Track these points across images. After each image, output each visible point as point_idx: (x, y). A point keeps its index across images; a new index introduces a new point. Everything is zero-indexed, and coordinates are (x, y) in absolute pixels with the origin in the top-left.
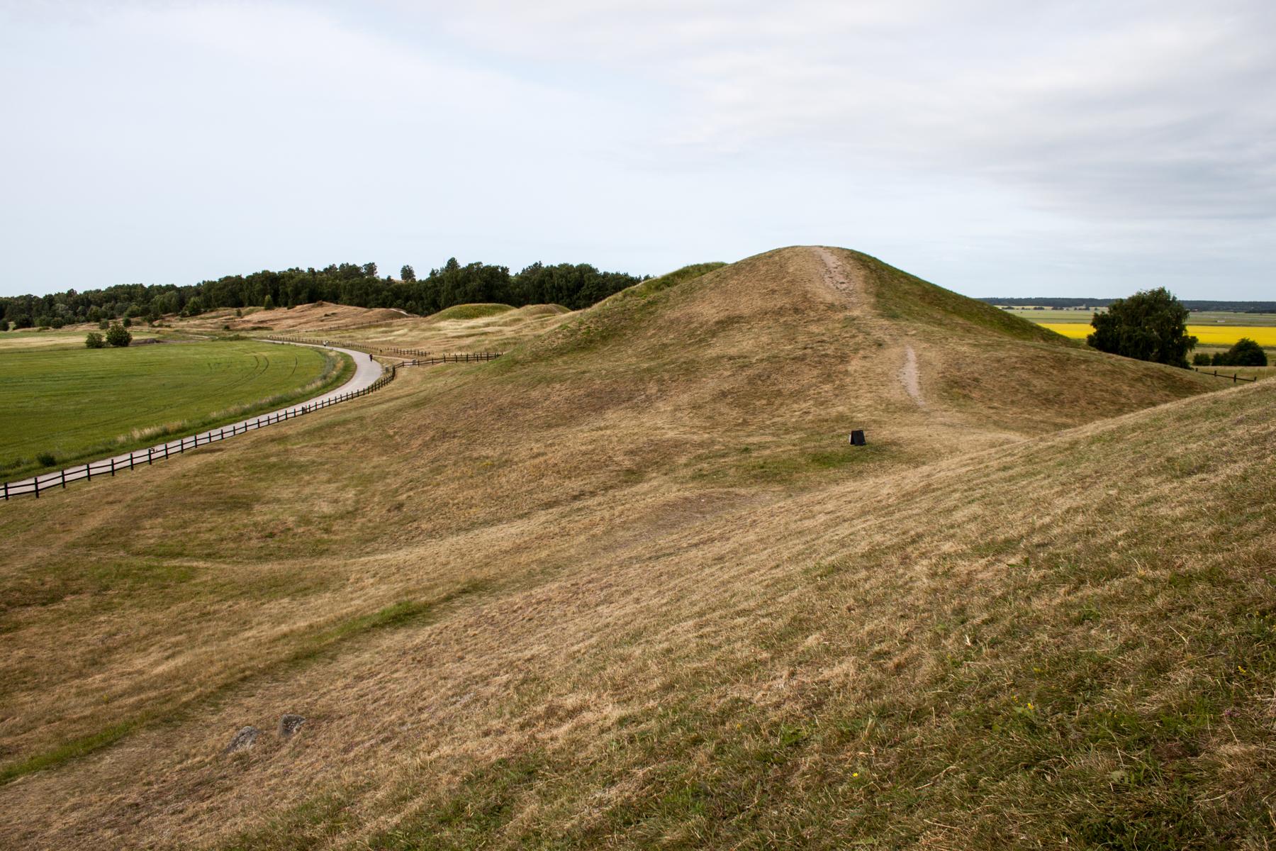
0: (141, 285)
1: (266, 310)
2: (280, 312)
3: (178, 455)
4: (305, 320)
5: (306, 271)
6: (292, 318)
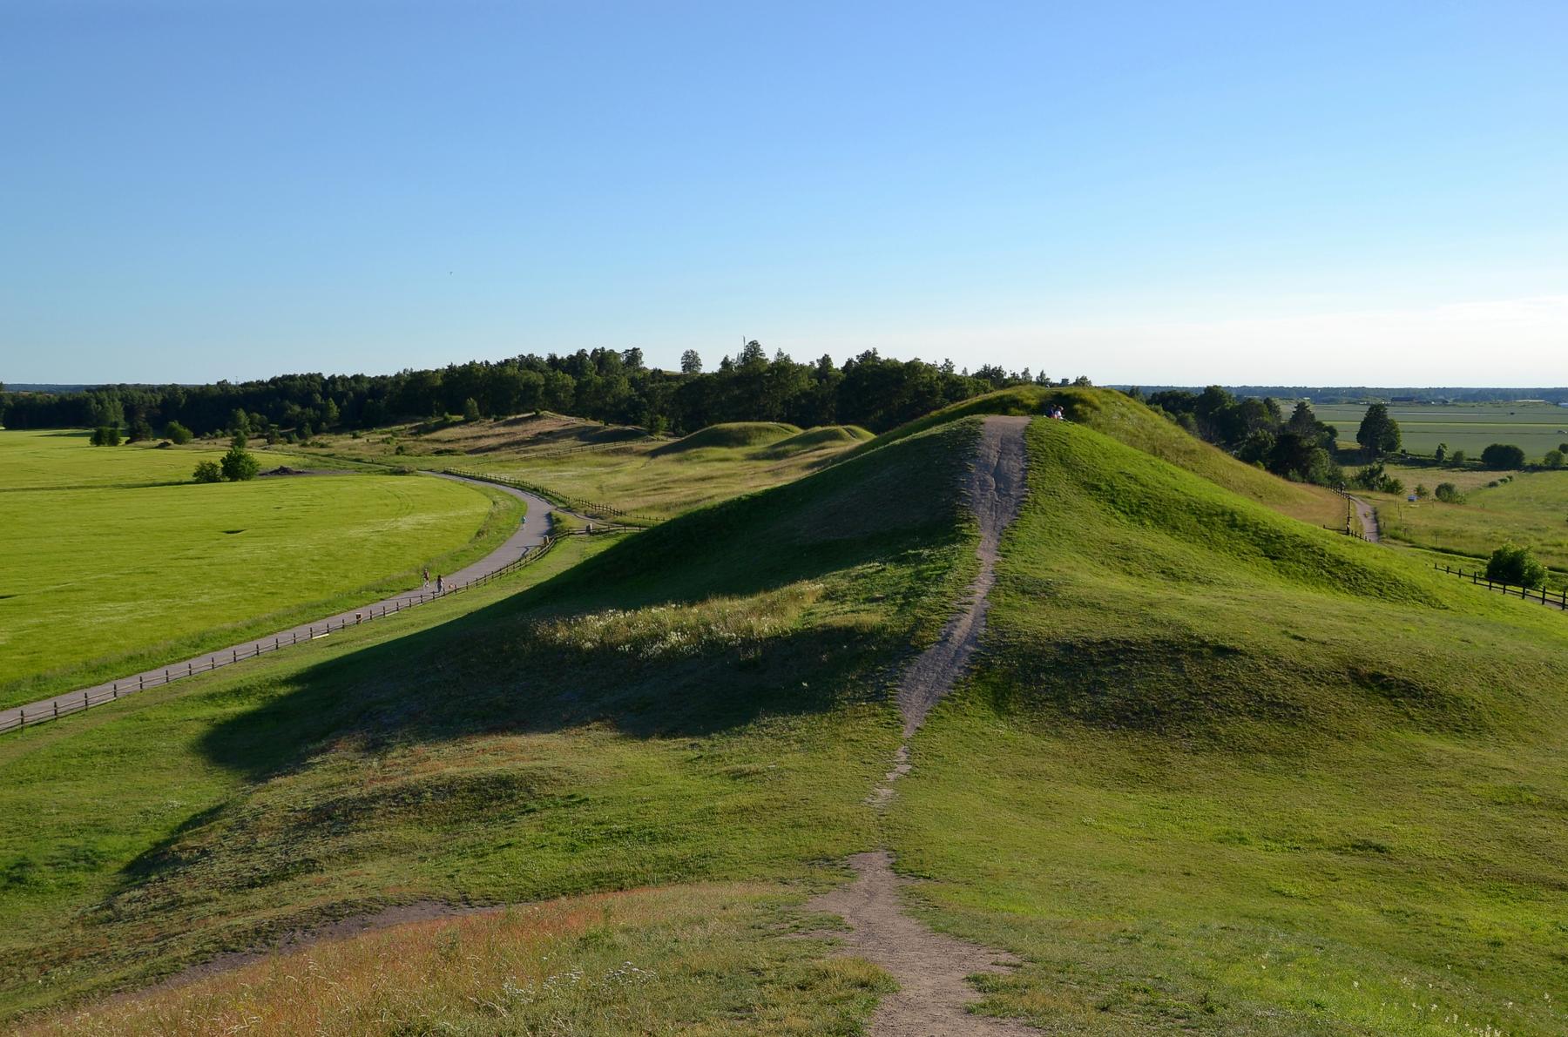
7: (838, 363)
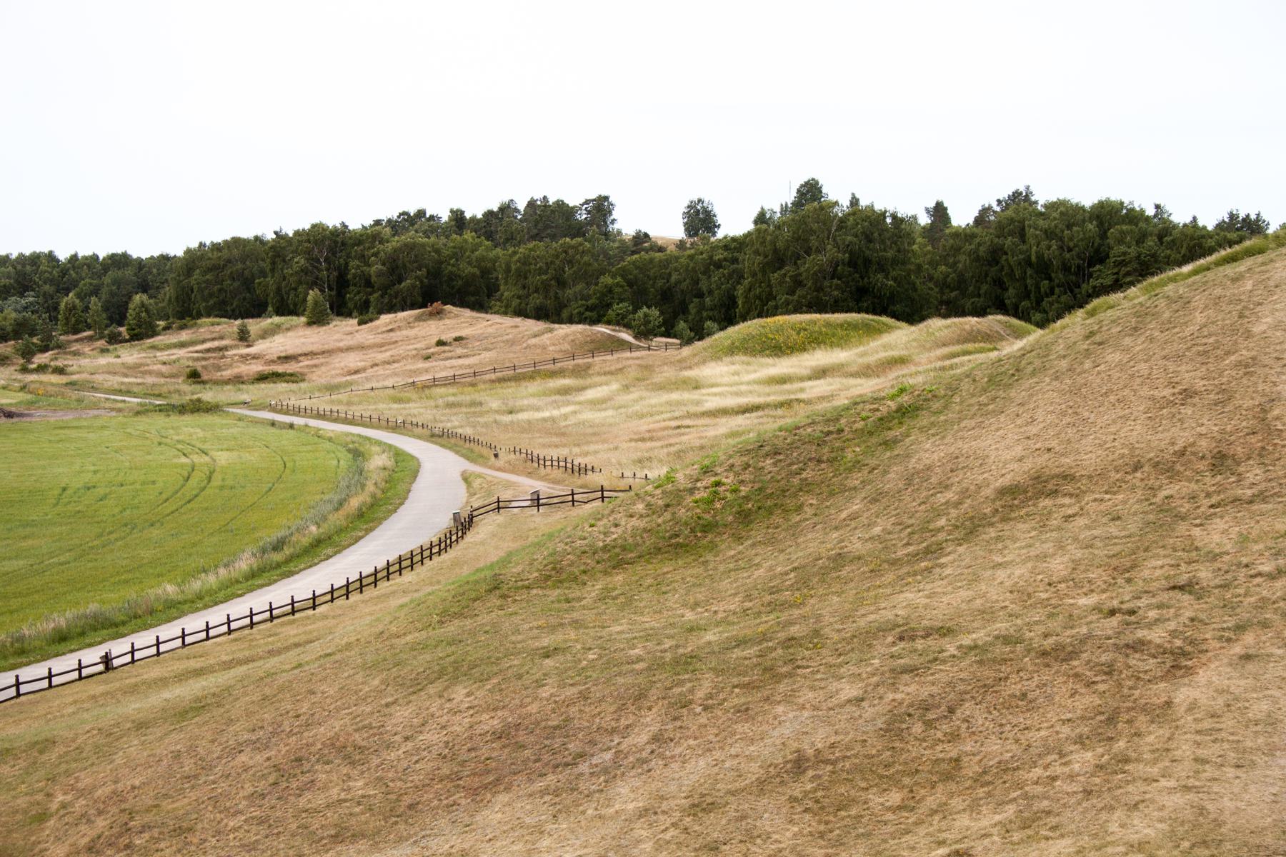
0: (51, 256)
1: (310, 324)
2: (343, 330)
3: (247, 631)
4: (386, 356)
5: (445, 217)
6: (361, 348)
7: (962, 217)
